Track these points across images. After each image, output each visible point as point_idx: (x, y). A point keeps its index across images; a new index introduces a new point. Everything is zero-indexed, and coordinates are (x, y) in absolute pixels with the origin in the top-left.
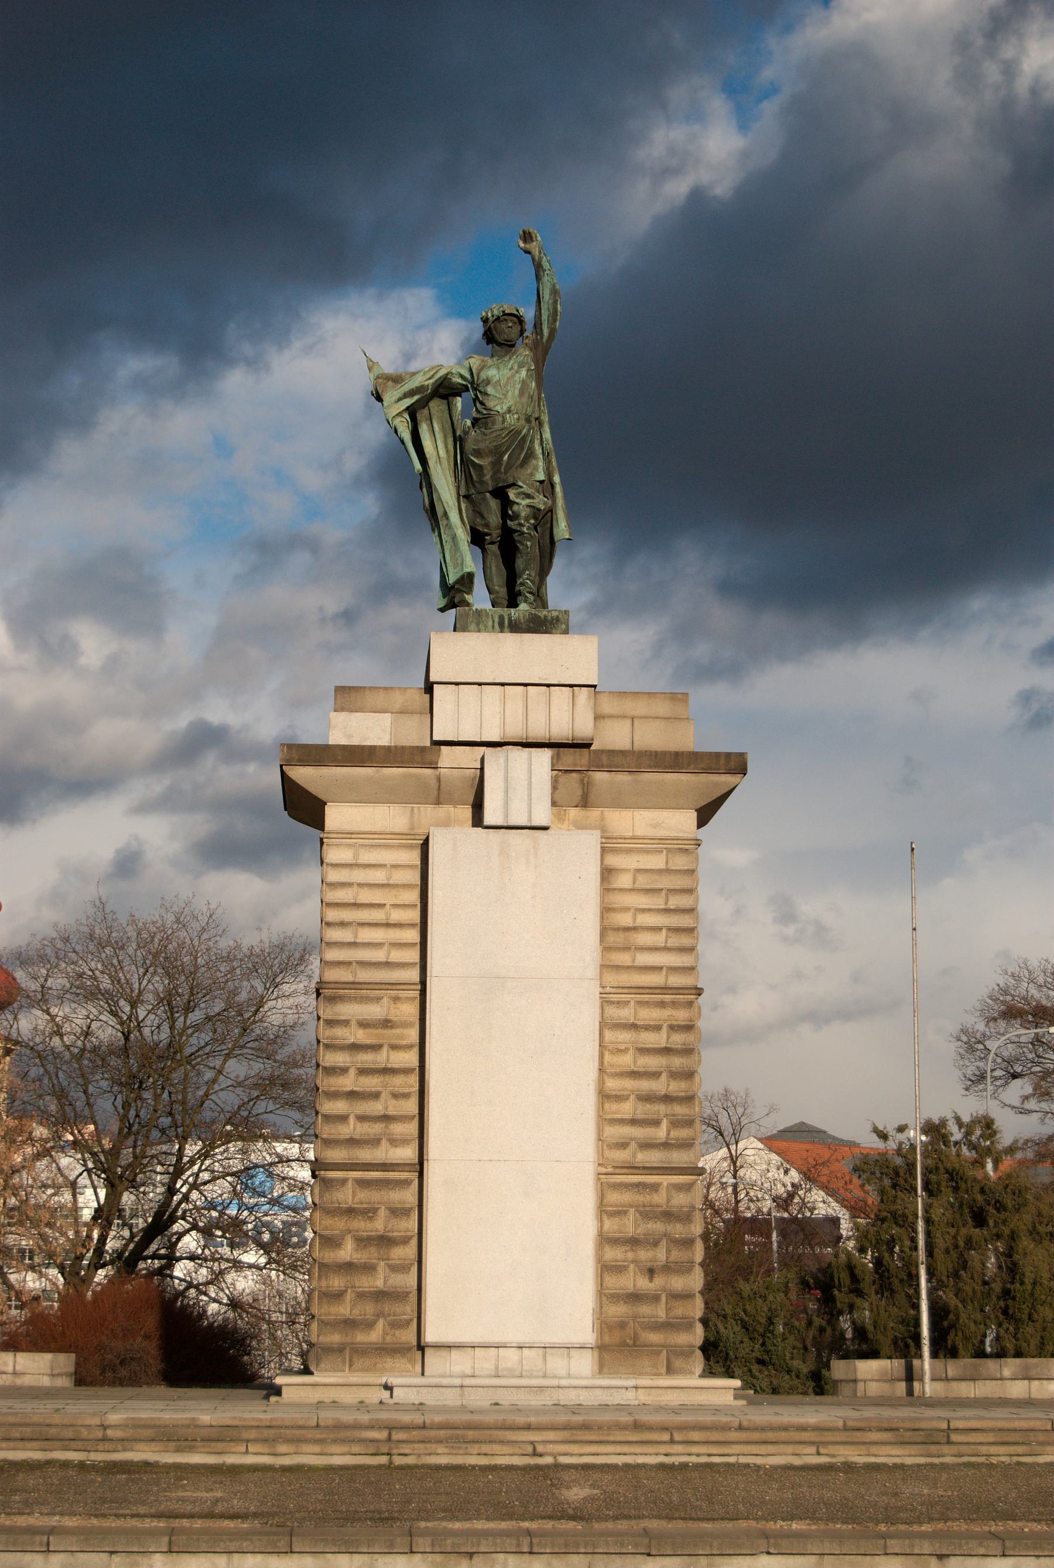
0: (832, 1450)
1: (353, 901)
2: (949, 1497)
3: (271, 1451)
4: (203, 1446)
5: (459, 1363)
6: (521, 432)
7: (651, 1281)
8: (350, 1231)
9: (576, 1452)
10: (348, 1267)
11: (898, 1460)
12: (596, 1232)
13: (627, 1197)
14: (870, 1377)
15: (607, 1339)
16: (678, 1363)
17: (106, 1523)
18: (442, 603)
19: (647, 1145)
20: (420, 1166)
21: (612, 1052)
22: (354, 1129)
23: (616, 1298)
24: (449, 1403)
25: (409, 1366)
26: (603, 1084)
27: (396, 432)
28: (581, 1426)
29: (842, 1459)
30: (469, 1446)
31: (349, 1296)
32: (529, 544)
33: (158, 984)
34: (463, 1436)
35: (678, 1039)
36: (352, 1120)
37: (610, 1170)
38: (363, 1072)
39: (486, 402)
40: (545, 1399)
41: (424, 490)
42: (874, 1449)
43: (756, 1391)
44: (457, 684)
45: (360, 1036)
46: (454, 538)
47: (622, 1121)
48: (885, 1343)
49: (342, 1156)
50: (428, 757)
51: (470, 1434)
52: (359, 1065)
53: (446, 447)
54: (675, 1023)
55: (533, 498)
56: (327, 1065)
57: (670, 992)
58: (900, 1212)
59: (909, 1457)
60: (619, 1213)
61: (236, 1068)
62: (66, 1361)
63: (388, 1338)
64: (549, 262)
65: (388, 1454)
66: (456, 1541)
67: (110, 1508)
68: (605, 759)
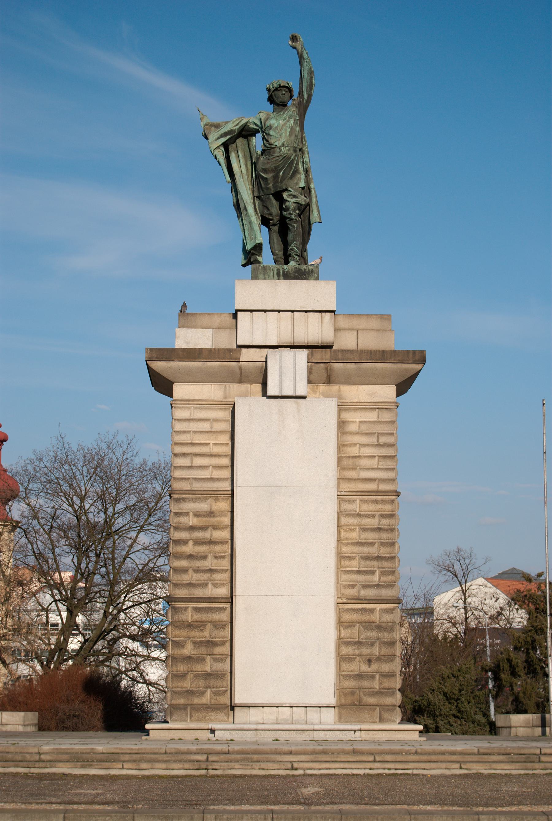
0: (469, 765)
1: (190, 441)
2: (528, 792)
3: (137, 767)
4: (97, 765)
5: (255, 715)
6: (290, 157)
7: (369, 667)
8: (190, 638)
9: (317, 767)
10: (189, 659)
11: (508, 772)
12: (336, 638)
13: (355, 617)
14: (519, 725)
15: (343, 701)
16: (386, 715)
17: (30, 807)
18: (244, 262)
19: (366, 586)
20: (231, 600)
21: (345, 530)
22: (192, 577)
23: (348, 677)
24: (248, 740)
25: (226, 718)
26: (341, 549)
27: (216, 158)
28: (321, 752)
29: (474, 771)
30: (254, 764)
31: (190, 676)
32: (295, 225)
33: (98, 487)
34: (251, 759)
35: (385, 522)
36: (190, 572)
37: (345, 601)
38: (197, 543)
39: (269, 139)
40: (307, 736)
41: (233, 193)
42: (494, 765)
43: (452, 734)
44: (251, 311)
45: (194, 521)
46: (250, 222)
47: (352, 572)
48: (531, 704)
49: (185, 593)
50: (234, 355)
51: (255, 757)
52: (194, 539)
53: (247, 167)
54: (384, 513)
55: (297, 198)
56: (176, 539)
57: (381, 494)
58: (539, 627)
59: (515, 770)
60: (351, 625)
61: (144, 539)
62: (33, 717)
63: (213, 701)
64: (307, 54)
65: (206, 769)
66: (229, 816)
67: (34, 799)
68: (340, 355)
